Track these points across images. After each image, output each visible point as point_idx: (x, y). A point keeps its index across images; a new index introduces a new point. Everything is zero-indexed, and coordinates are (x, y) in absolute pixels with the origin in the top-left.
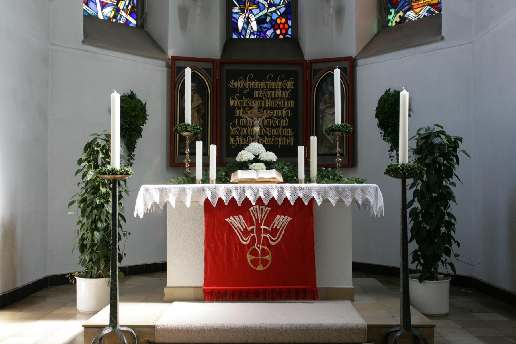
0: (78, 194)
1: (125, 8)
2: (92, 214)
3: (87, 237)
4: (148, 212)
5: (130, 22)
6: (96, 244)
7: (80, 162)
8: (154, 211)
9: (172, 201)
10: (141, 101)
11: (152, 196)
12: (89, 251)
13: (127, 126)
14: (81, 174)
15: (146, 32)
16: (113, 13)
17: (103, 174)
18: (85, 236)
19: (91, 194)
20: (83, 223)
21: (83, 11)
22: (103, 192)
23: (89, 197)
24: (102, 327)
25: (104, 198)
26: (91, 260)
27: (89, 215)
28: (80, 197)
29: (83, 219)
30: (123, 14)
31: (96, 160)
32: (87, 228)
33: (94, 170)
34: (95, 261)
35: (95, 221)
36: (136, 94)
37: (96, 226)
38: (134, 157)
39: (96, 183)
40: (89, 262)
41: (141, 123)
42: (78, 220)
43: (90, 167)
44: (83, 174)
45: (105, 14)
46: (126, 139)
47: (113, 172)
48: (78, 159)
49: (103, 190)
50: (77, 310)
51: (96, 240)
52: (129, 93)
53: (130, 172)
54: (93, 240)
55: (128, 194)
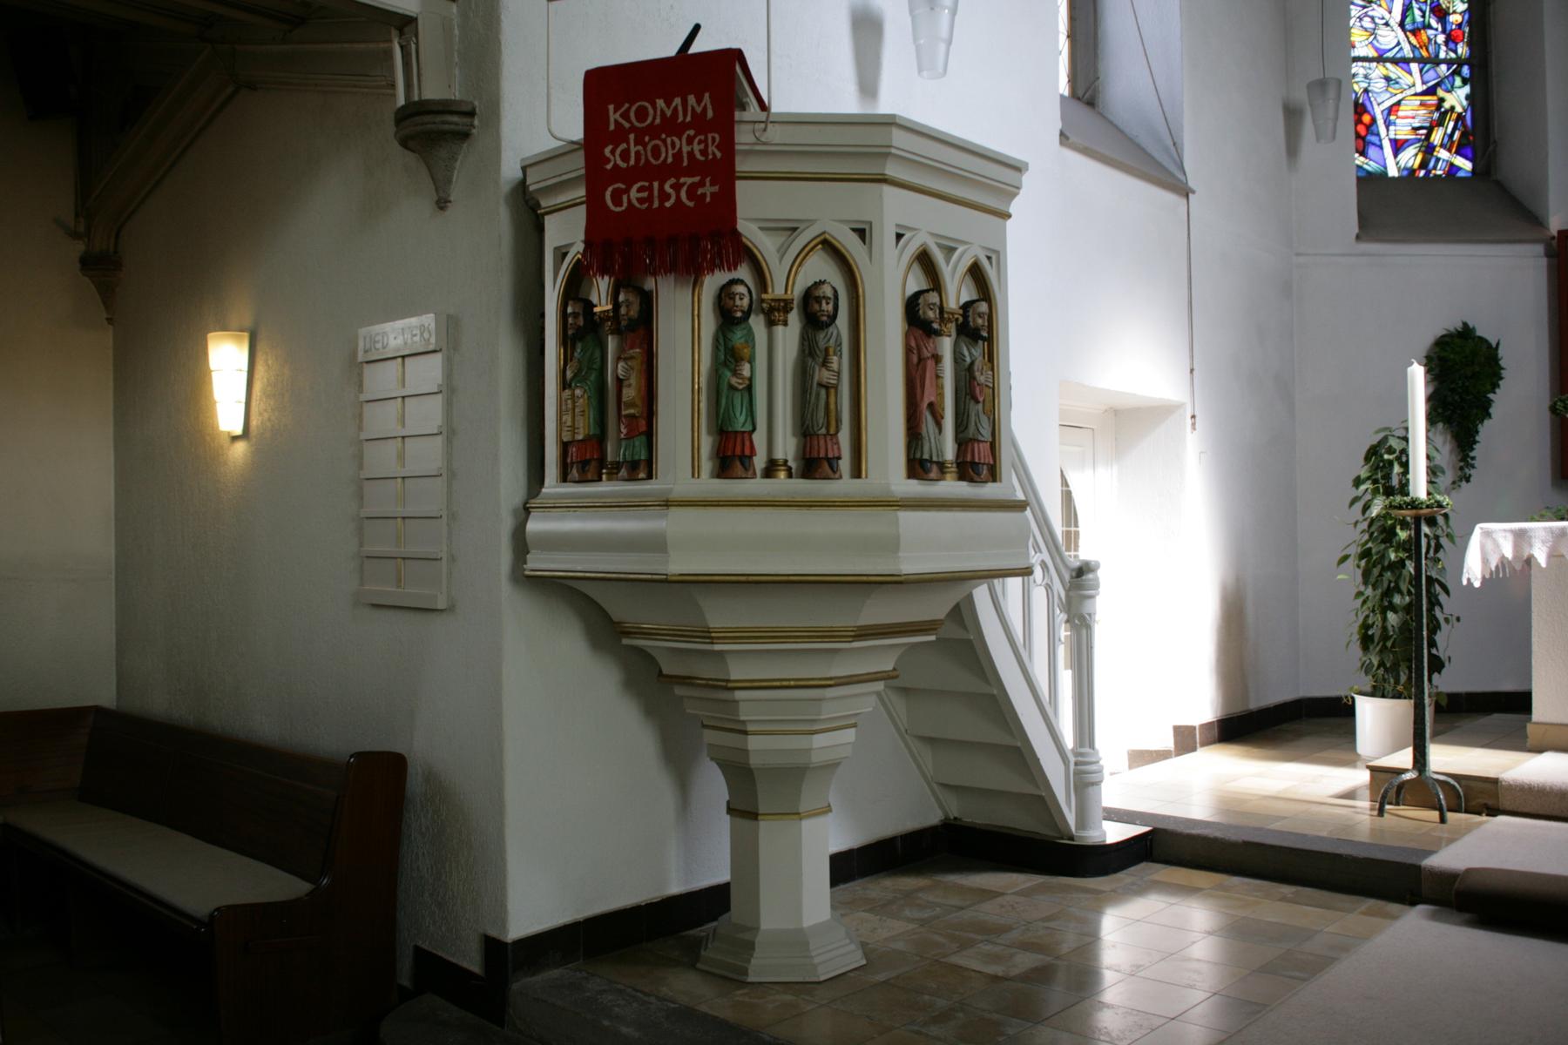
0: (1355, 541)
1: (1446, 139)
2: (1382, 580)
3: (1374, 623)
4: (1501, 575)
5: (1459, 169)
6: (1392, 636)
7: (1358, 482)
8: (1508, 575)
9: (1540, 555)
10: (1486, 341)
11: (1497, 546)
12: (1378, 649)
13: (1457, 398)
14: (1359, 506)
15: (1499, 184)
16: (1420, 157)
17: (1395, 507)
18: (1370, 622)
19: (1381, 543)
20: (1366, 595)
21: (1354, 169)
22: (1402, 538)
23: (1375, 548)
24: (1400, 772)
25: (1405, 550)
26: (1382, 664)
27: (1377, 581)
28: (1359, 548)
29: (1366, 589)
30: (1443, 154)
31: (1388, 477)
32: (1374, 606)
33: (1384, 498)
34: (1391, 666)
35: (1388, 593)
36: (1474, 328)
37: (1390, 603)
38: (1473, 462)
39: (1390, 522)
40: (1378, 668)
41: (1489, 387)
42: (1356, 590)
43: (1375, 492)
44: (1365, 506)
45: (1402, 164)
46: (1454, 424)
47: (1414, 505)
48: (1354, 477)
49: (1403, 535)
50: (1359, 755)
51: (1390, 628)
52: (1459, 326)
53: (1445, 504)
54: (1384, 628)
55: (1452, 541)
